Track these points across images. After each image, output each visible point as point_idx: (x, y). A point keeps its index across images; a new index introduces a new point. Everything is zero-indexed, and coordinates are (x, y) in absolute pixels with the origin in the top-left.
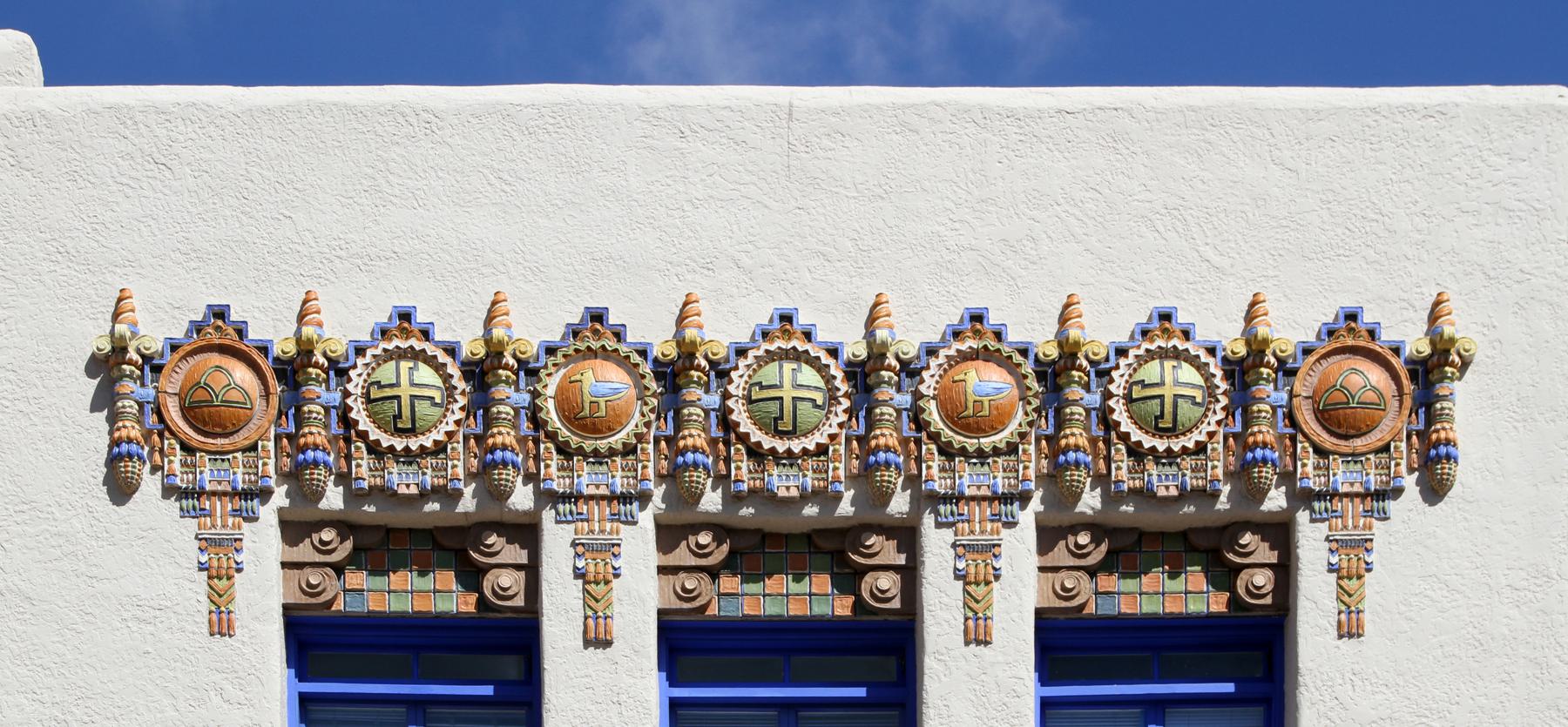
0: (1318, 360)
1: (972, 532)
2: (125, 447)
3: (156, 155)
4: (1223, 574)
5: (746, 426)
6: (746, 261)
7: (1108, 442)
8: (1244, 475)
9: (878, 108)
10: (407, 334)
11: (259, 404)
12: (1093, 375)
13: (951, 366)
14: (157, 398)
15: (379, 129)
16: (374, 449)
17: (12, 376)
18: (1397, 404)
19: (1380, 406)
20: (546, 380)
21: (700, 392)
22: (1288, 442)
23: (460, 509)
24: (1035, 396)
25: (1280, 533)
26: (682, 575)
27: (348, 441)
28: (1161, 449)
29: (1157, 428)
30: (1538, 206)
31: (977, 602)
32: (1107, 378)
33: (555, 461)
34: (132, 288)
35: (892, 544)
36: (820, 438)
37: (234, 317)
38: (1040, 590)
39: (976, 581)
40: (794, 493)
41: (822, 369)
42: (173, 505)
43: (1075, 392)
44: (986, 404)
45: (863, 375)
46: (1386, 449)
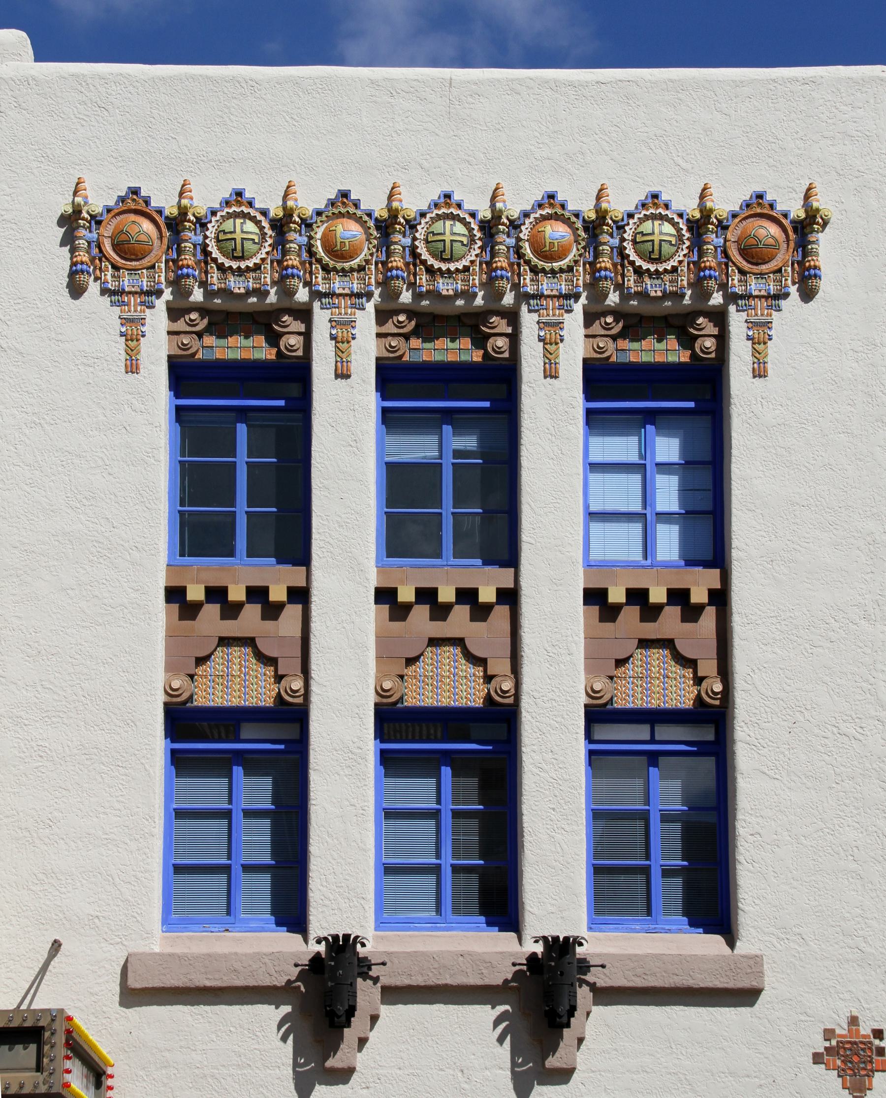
0: (740, 221)
1: (548, 315)
2: (79, 267)
3: (99, 103)
4: (688, 341)
5: (425, 256)
6: (426, 164)
7: (623, 266)
8: (699, 286)
9: (499, 81)
10: (240, 204)
11: (156, 242)
12: (614, 228)
13: (537, 223)
14: (98, 239)
15: (225, 89)
16: (221, 268)
17: (14, 226)
18: (785, 246)
19: (776, 246)
20: (316, 229)
21: (400, 237)
22: (723, 266)
23: (268, 301)
24: (583, 240)
25: (720, 317)
26: (390, 338)
27: (206, 263)
28: (652, 270)
29: (650, 258)
30: (868, 134)
31: (551, 354)
32: (622, 231)
33: (321, 275)
34: (85, 177)
35: (504, 321)
36: (465, 262)
37: (143, 194)
38: (586, 348)
39: (551, 342)
40: (451, 293)
41: (466, 224)
42: (106, 300)
43: (605, 238)
44: (556, 244)
45: (489, 228)
46: (779, 271)
